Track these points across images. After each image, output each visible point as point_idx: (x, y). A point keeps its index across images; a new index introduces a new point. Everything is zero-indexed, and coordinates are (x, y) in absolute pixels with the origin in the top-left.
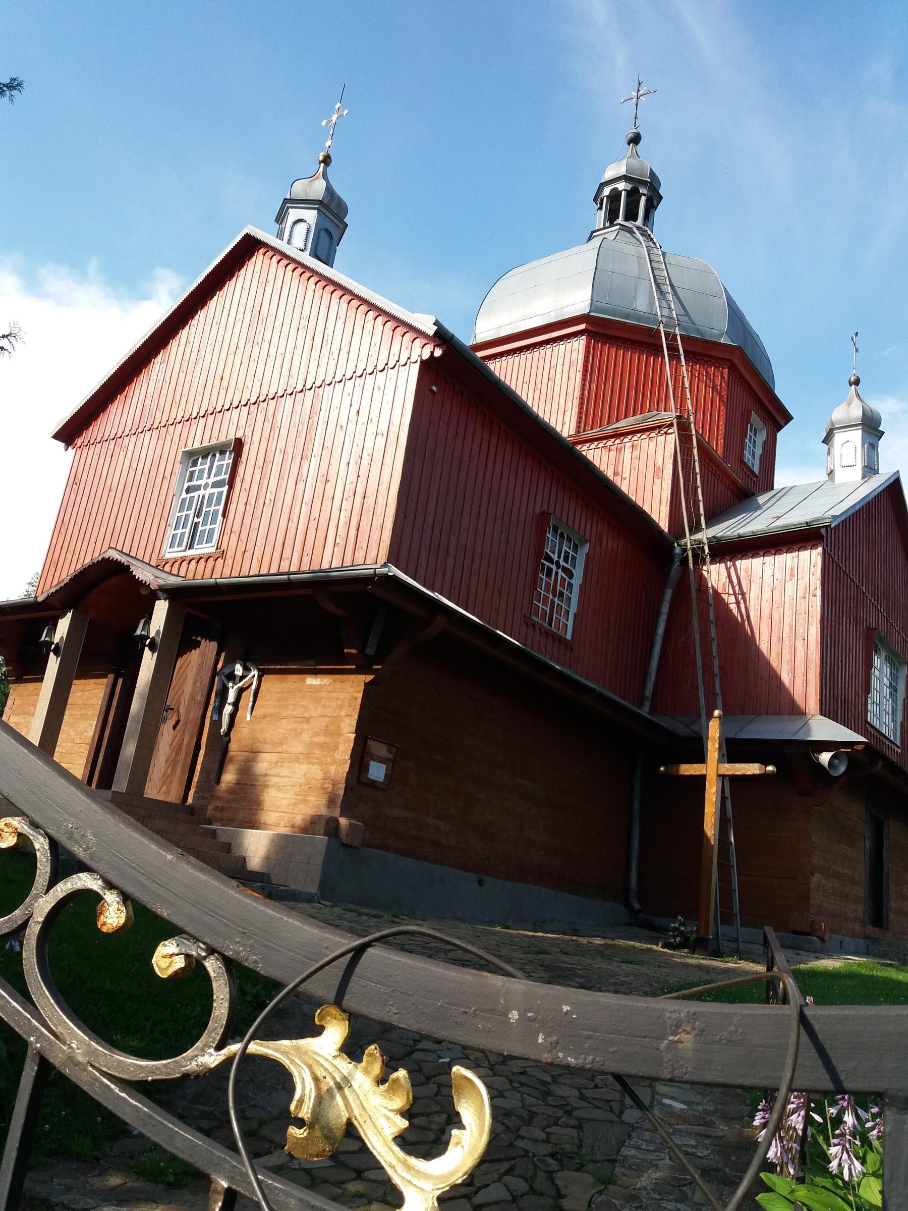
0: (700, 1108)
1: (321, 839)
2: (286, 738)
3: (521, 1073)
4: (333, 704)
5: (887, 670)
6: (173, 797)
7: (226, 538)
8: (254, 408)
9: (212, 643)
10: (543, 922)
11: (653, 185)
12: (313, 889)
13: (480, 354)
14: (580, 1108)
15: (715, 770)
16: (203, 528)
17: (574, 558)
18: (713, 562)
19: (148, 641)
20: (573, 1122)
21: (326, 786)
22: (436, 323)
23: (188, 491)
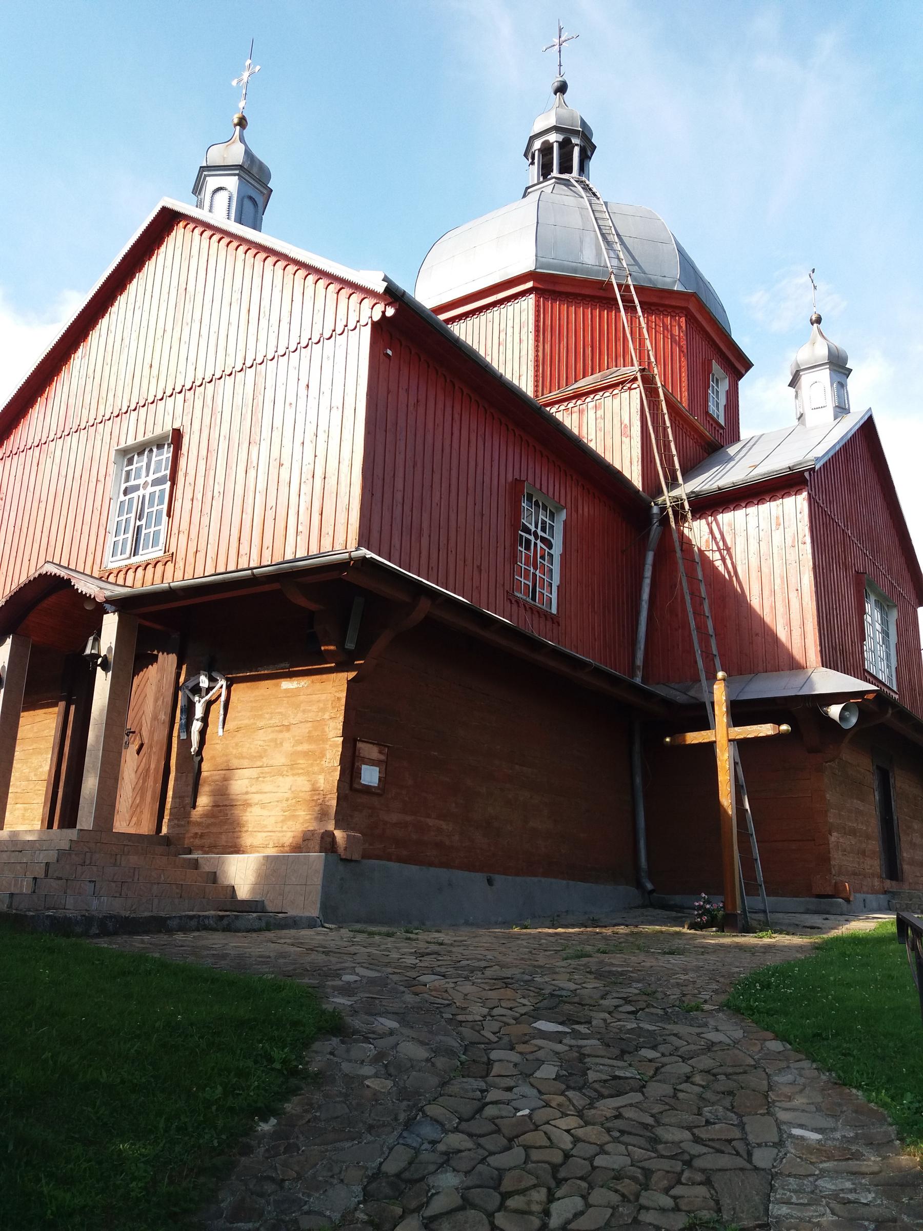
0: (838, 1135)
1: (317, 857)
2: (265, 750)
3: (616, 1117)
4: (314, 708)
5: (877, 615)
6: (146, 827)
9: (170, 655)
10: (558, 916)
11: (585, 134)
12: (314, 911)
14: (699, 1156)
15: (725, 735)
16: (147, 531)
17: (552, 527)
18: (694, 518)
19: (100, 661)
20: (699, 1177)
21: (315, 798)
22: (385, 279)
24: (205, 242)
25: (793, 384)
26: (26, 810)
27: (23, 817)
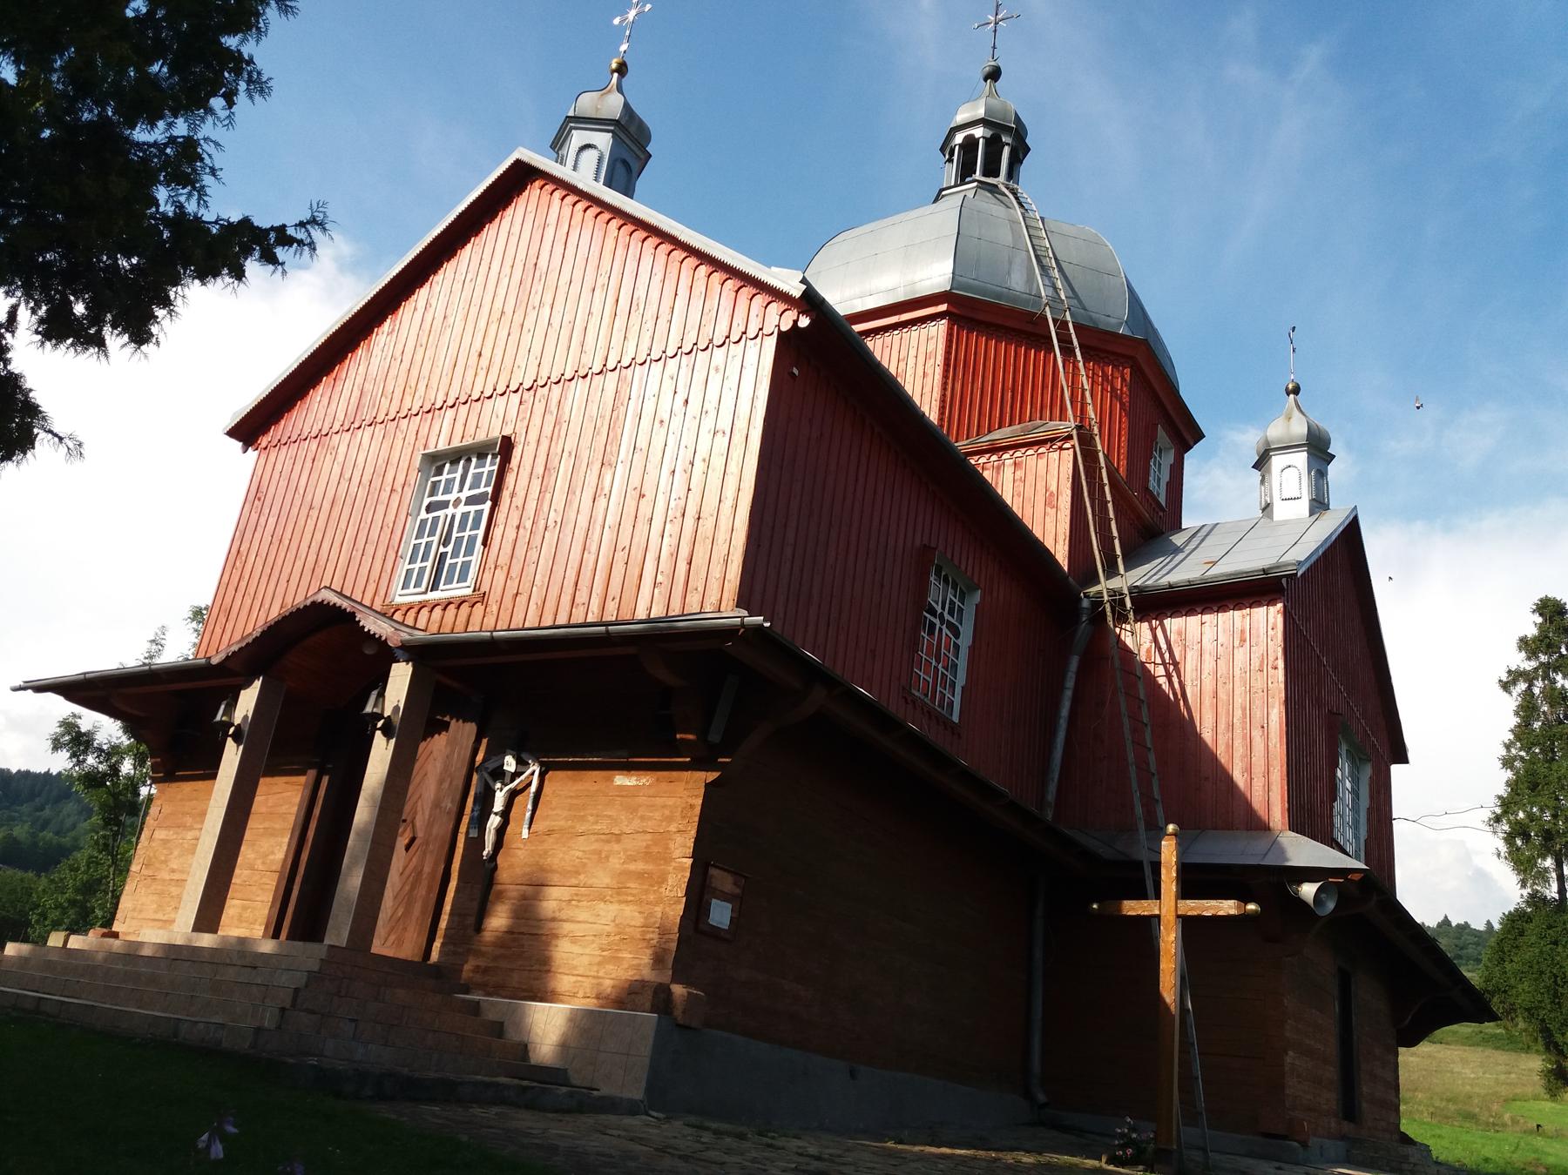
2: (585, 865)
4: (657, 815)
6: (408, 950)
7: (487, 576)
8: (528, 396)
12: (637, 1093)
13: (857, 328)
17: (961, 610)
18: (1140, 618)
19: (232, 730)
21: (648, 936)
22: (804, 281)
23: (428, 510)
24: (567, 210)
25: (1259, 465)
26: (245, 908)
27: (240, 919)
